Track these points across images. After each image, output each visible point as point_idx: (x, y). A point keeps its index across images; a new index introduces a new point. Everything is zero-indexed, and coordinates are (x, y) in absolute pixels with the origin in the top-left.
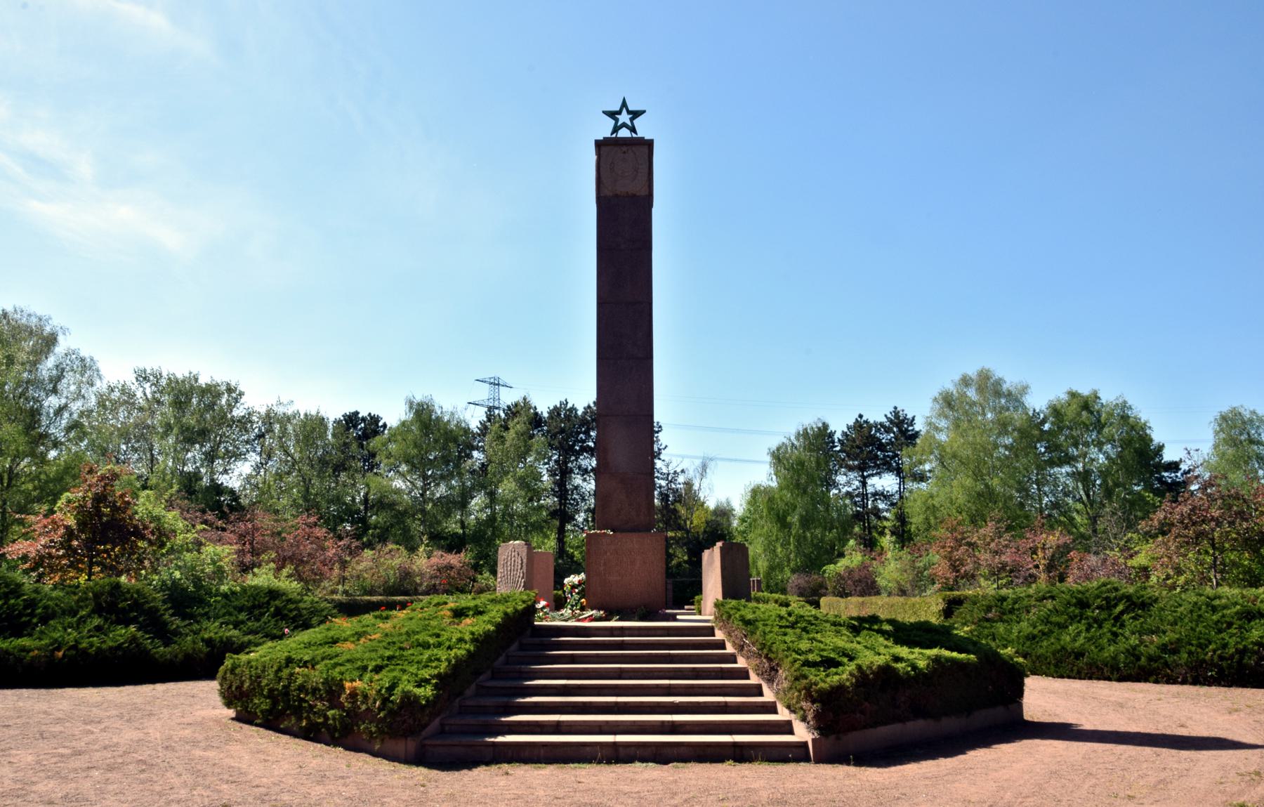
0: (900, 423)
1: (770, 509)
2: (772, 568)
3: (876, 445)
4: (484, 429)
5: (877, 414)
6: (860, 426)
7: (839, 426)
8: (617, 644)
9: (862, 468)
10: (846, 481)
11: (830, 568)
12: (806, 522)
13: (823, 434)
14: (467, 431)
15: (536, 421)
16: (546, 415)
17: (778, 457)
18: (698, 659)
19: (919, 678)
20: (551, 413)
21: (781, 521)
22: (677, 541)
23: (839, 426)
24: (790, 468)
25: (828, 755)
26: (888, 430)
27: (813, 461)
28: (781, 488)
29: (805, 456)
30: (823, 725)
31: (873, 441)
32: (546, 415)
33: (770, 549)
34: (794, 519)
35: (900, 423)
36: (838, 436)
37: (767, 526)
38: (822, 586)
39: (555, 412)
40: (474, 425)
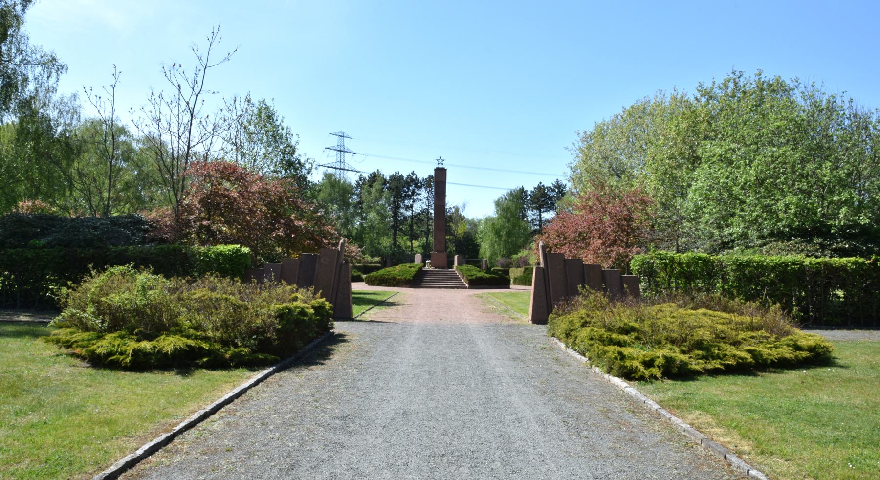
0: (559, 187)
1: (493, 228)
2: (492, 255)
3: (543, 198)
4: (358, 185)
5: (548, 183)
6: (540, 189)
7: (530, 188)
8: (438, 274)
9: (539, 209)
10: (531, 214)
11: (515, 256)
12: (509, 234)
13: (522, 191)
14: (350, 185)
15: (385, 182)
16: (388, 178)
17: (498, 204)
18: (453, 276)
19: (487, 278)
20: (391, 177)
21: (497, 233)
22: (450, 240)
23: (530, 188)
24: (503, 210)
25: (470, 288)
26: (553, 190)
27: (516, 204)
28: (498, 219)
29: (510, 204)
30: (469, 284)
31: (545, 195)
32: (388, 178)
33: (492, 246)
34: (503, 233)
35: (559, 187)
36: (529, 193)
37: (491, 235)
38: (511, 263)
39: (393, 177)
40: (354, 183)
